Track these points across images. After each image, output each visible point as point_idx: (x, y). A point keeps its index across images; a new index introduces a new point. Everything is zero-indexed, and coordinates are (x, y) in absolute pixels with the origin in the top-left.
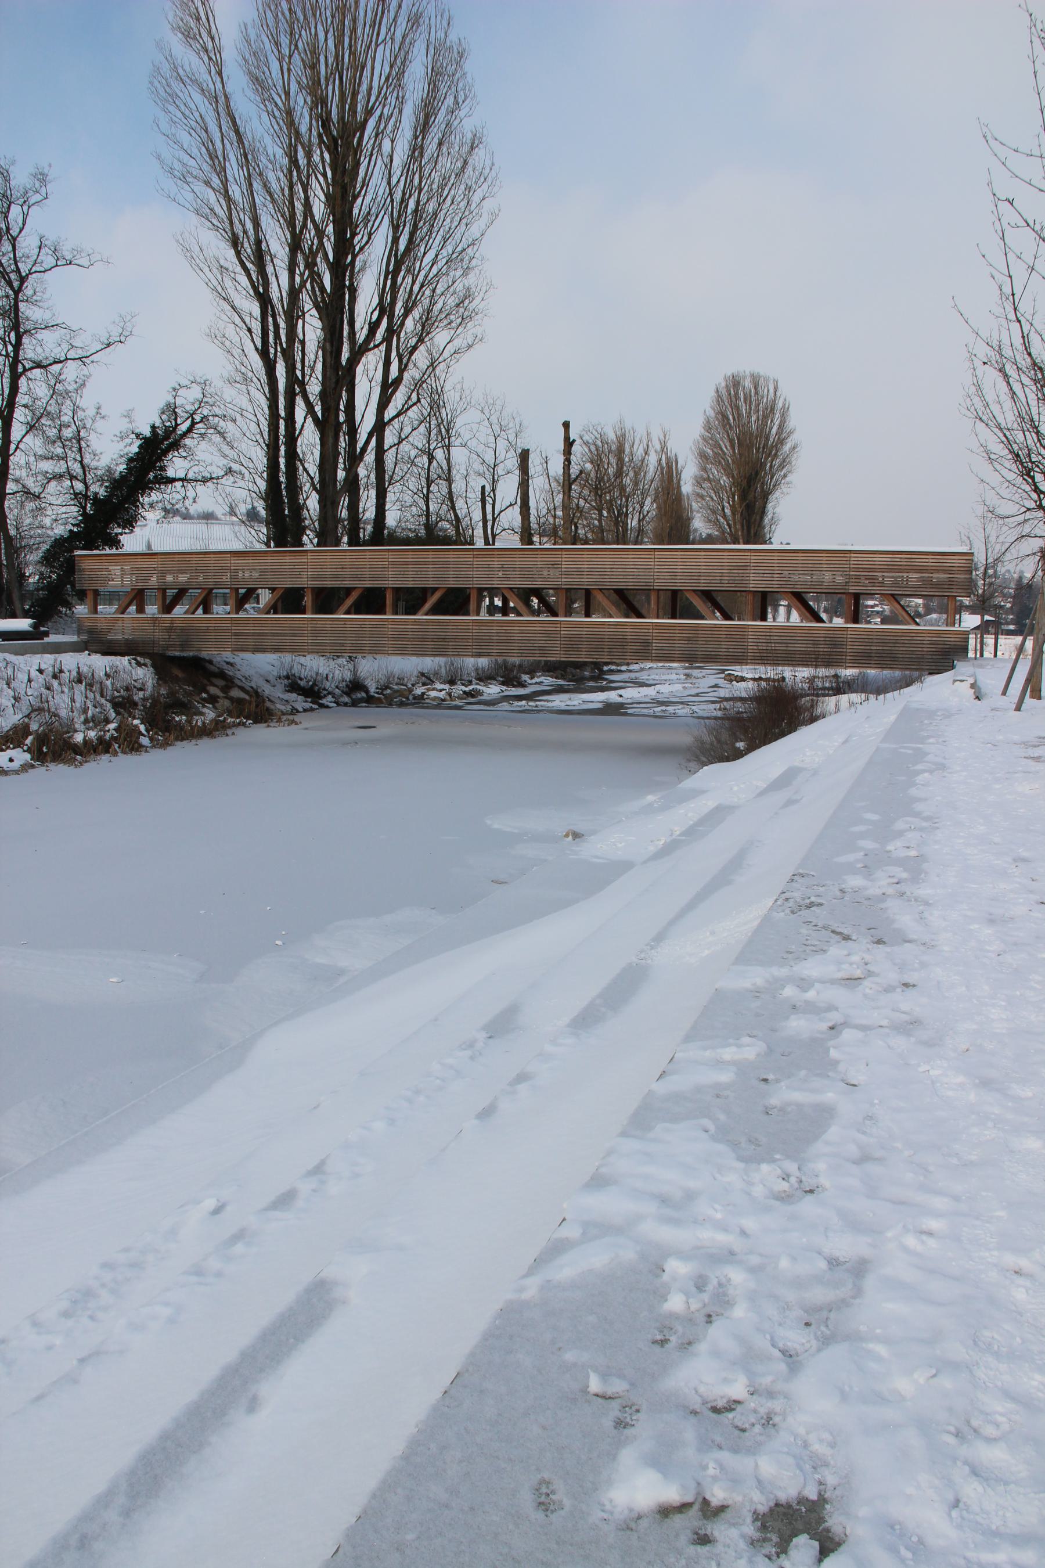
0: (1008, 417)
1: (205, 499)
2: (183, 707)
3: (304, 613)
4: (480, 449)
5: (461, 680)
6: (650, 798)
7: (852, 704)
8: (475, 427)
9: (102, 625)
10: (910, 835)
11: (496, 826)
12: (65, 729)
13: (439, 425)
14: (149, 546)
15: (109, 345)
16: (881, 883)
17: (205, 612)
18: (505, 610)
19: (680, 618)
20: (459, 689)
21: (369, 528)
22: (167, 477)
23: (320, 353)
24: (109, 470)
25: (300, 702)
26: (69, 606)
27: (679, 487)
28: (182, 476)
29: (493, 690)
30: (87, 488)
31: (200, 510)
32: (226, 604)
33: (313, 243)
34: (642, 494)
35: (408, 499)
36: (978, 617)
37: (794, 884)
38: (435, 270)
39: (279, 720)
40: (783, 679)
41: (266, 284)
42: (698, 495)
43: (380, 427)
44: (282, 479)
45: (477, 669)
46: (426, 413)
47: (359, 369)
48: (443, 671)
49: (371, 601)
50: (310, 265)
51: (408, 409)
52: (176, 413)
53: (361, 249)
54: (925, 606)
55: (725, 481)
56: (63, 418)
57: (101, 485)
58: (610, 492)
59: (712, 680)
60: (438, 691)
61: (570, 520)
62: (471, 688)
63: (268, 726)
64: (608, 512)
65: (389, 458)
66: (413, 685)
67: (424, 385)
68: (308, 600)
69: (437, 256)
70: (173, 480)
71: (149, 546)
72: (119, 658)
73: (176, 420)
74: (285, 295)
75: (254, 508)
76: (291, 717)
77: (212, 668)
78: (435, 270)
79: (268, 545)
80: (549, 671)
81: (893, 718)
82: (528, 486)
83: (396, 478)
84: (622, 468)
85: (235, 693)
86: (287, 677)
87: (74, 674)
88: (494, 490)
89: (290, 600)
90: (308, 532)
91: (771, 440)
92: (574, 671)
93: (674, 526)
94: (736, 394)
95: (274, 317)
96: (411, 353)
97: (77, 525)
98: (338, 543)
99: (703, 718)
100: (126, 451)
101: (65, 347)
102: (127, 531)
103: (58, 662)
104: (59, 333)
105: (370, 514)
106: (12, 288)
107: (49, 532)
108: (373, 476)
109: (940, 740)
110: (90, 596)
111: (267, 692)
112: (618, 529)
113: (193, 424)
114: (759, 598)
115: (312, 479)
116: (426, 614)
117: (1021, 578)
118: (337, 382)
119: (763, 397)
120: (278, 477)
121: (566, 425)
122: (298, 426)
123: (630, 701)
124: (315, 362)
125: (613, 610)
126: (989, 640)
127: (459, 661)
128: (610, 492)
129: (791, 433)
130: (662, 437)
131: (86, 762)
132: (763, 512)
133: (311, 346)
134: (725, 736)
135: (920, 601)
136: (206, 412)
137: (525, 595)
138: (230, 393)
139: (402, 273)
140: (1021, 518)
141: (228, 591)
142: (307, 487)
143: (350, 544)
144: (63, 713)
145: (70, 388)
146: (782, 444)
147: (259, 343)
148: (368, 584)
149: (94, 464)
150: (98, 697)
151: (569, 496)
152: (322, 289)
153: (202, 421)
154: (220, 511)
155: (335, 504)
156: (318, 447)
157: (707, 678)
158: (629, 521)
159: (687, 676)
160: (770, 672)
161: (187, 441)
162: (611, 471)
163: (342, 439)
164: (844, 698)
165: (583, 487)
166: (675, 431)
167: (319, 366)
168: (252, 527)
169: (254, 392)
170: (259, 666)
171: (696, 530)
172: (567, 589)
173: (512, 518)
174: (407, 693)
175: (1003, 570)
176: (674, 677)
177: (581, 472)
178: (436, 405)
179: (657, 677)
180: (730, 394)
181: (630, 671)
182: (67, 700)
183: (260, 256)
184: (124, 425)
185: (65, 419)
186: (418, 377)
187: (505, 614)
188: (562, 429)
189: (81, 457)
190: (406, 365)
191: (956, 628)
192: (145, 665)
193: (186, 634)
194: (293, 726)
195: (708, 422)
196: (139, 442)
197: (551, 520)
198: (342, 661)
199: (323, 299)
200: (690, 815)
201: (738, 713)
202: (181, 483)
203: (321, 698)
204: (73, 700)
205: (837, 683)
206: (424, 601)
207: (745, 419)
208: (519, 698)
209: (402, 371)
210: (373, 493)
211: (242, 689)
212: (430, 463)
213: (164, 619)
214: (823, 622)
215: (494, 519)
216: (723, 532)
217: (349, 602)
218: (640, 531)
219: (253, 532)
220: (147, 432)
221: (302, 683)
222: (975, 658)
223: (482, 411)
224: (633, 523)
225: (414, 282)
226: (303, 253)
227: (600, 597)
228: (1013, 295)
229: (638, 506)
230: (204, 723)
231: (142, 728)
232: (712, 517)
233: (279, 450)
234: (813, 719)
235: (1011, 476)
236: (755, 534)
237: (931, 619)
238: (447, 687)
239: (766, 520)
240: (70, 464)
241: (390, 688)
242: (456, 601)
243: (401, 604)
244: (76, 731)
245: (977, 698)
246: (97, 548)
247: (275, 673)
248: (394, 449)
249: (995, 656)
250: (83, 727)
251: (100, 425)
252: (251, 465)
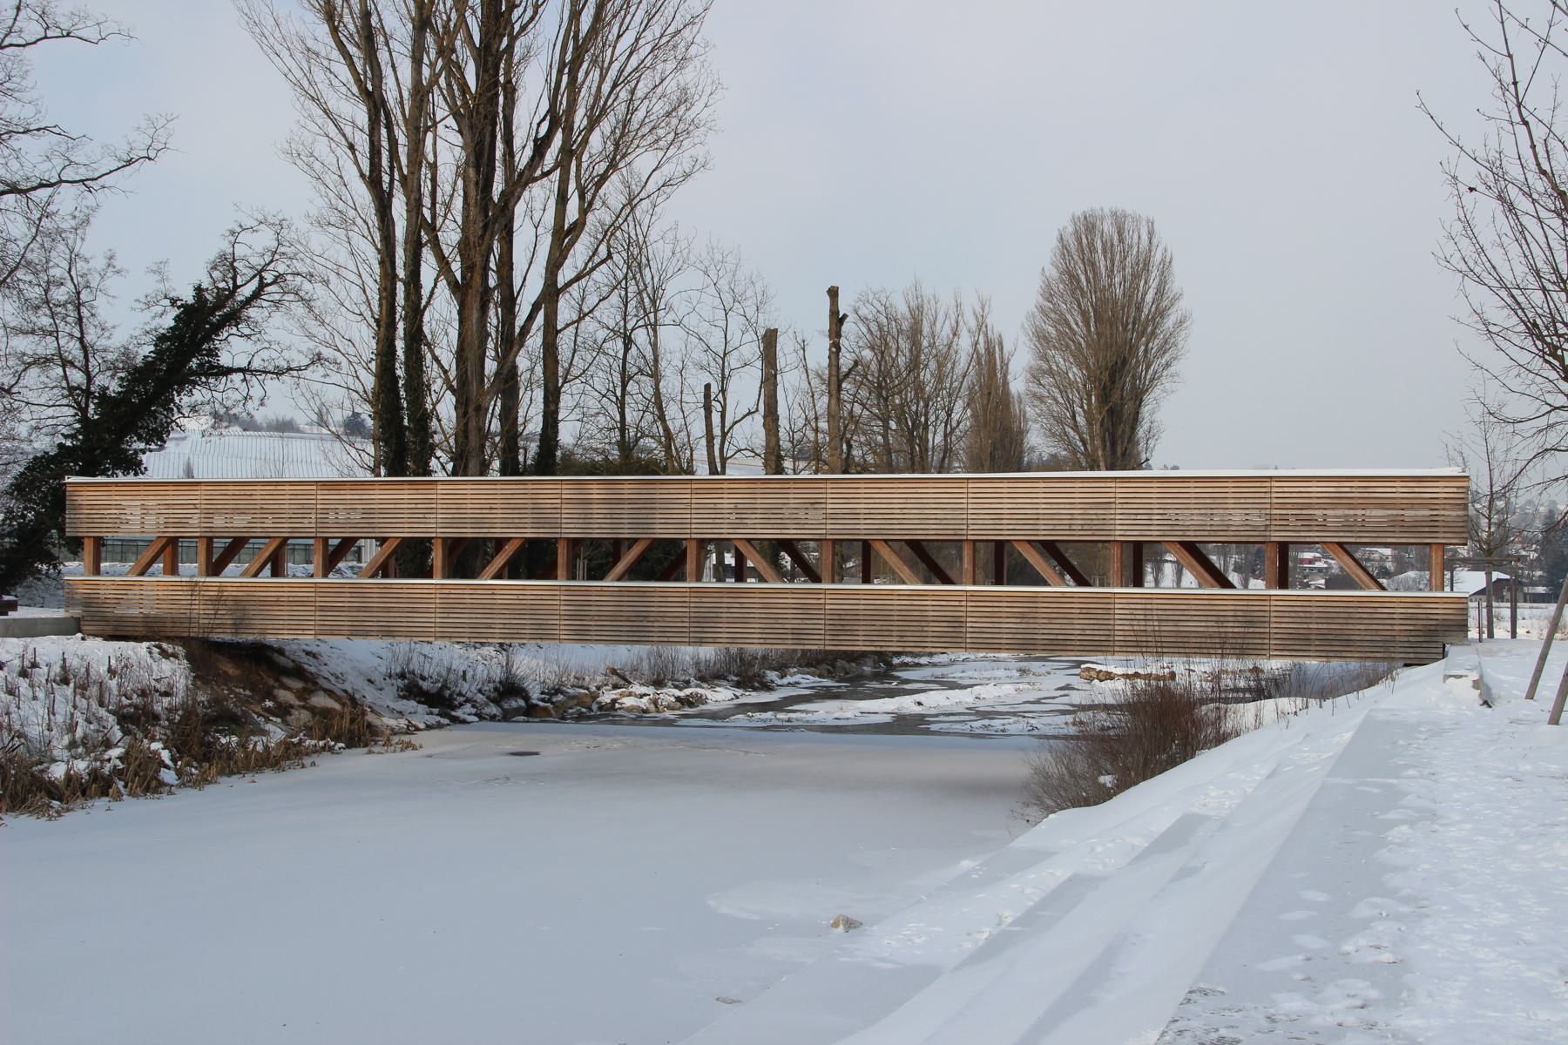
0: (1514, 269)
1: (279, 400)
2: (233, 722)
3: (431, 577)
4: (703, 329)
5: (672, 679)
6: (966, 864)
7: (1281, 715)
8: (695, 295)
9: (103, 593)
10: (1380, 927)
11: (724, 910)
12: (36, 758)
13: (640, 293)
14: (189, 471)
15: (129, 163)
16: (1333, 1008)
17: (275, 574)
18: (740, 573)
19: (1009, 584)
20: (669, 694)
21: (533, 447)
22: (219, 367)
23: (460, 183)
24: (126, 353)
25: (420, 714)
26: (52, 560)
27: (1005, 383)
28: (244, 364)
29: (720, 696)
30: (90, 379)
31: (272, 417)
32: (309, 562)
33: (449, 19)
34: (950, 395)
35: (592, 404)
36: (1482, 575)
37: (1191, 1007)
38: (634, 62)
39: (388, 743)
40: (1173, 675)
41: (378, 77)
42: (1034, 395)
43: (551, 294)
44: (400, 372)
45: (697, 664)
46: (620, 275)
47: (520, 209)
48: (645, 665)
49: (534, 559)
50: (446, 51)
51: (593, 269)
52: (234, 269)
53: (523, 28)
54: (1395, 558)
55: (1075, 373)
56: (52, 272)
57: (113, 377)
58: (900, 393)
59: (1061, 679)
60: (636, 697)
61: (841, 435)
62: (688, 691)
63: (370, 752)
64: (898, 423)
65: (565, 342)
66: (599, 688)
67: (618, 233)
68: (437, 557)
69: (637, 40)
70: (228, 371)
71: (189, 471)
72: (132, 644)
73: (234, 279)
74: (406, 95)
75: (356, 415)
76: (406, 738)
77: (282, 660)
78: (634, 62)
79: (375, 471)
80: (809, 665)
81: (1347, 736)
82: (776, 385)
83: (575, 372)
84: (918, 356)
85: (320, 700)
86: (402, 676)
87: (57, 669)
88: (723, 391)
89: (409, 557)
90: (439, 453)
91: (1146, 311)
92: (847, 665)
93: (1000, 447)
94: (1091, 245)
95: (389, 127)
96: (599, 185)
97: (72, 437)
98: (484, 469)
99: (1048, 737)
100: (154, 324)
101: (59, 162)
102: (153, 446)
103: (30, 651)
104: (47, 140)
105: (535, 425)
107: (24, 446)
108: (539, 370)
109: (1426, 772)
110: (89, 546)
111: (369, 699)
112: (913, 448)
113: (262, 285)
114: (1130, 551)
115: (445, 372)
116: (619, 579)
117: (1551, 513)
118: (485, 228)
119: (1131, 247)
120: (393, 369)
121: (833, 293)
122: (425, 292)
123: (933, 712)
124: (452, 196)
125: (905, 571)
126: (1503, 610)
127: (668, 651)
128: (900, 393)
129: (1175, 299)
130: (978, 309)
131: (68, 810)
132: (1135, 419)
133: (446, 173)
134: (1081, 766)
135: (1387, 552)
136: (281, 268)
137: (774, 548)
138: (319, 241)
139: (585, 65)
140: (1543, 422)
141: (311, 541)
142: (437, 385)
143: (503, 472)
144: (34, 731)
145: (64, 226)
146: (1162, 317)
148: (530, 533)
149: (101, 343)
150: (95, 705)
151: (839, 399)
152: (464, 87)
154: (301, 420)
155: (481, 410)
156: (456, 324)
157: (1050, 679)
158: (930, 436)
159: (1023, 671)
160: (1153, 666)
161: (252, 312)
162: (901, 361)
163: (492, 312)
164: (1269, 705)
165: (859, 385)
166: (998, 298)
167: (458, 203)
168: (352, 445)
169: (357, 239)
170: (357, 658)
171: (1032, 449)
172: (834, 541)
173: (751, 432)
174: (588, 700)
175: (1521, 501)
176: (1001, 673)
177: (856, 363)
178: (636, 265)
179: (976, 675)
180: (1080, 243)
181: (934, 665)
182: (43, 711)
183: (369, 36)
184: (151, 285)
185: (57, 272)
186: (608, 221)
187: (740, 579)
188: (827, 299)
189: (82, 332)
190: (591, 204)
191: (1447, 593)
192: (175, 656)
193: (240, 607)
194: (410, 753)
195: (1049, 286)
196: (176, 312)
197: (811, 436)
198: (489, 651)
199: (465, 103)
200: (1028, 891)
201: (1103, 729)
202: (241, 376)
203: (454, 708)
204: (52, 712)
205: (1258, 680)
206: (617, 559)
207: (1105, 281)
208: (764, 707)
209: (584, 211)
210: (539, 394)
211: (330, 693)
212: (627, 350)
213: (206, 585)
214: (1232, 586)
215: (724, 435)
216: (1074, 452)
217: (499, 561)
218: (947, 450)
219: (353, 452)
220: (188, 297)
221: (425, 685)
222: (1480, 640)
223: (706, 273)
224: (936, 438)
225: (602, 79)
226: (436, 33)
227: (885, 553)
228: (1515, 83)
229: (943, 414)
230: (266, 747)
231: (165, 755)
232: (1057, 429)
233: (395, 329)
234: (1221, 739)
235: (1524, 358)
236: (1124, 454)
237: (1406, 579)
238: (650, 690)
239: (1141, 433)
240: (62, 342)
241: (562, 693)
242: (665, 560)
243: (581, 565)
244: (54, 761)
245: (1486, 703)
246: (103, 473)
247: (383, 670)
248: (572, 329)
249: (1514, 635)
250: (66, 754)
251: (112, 283)
252: (352, 351)
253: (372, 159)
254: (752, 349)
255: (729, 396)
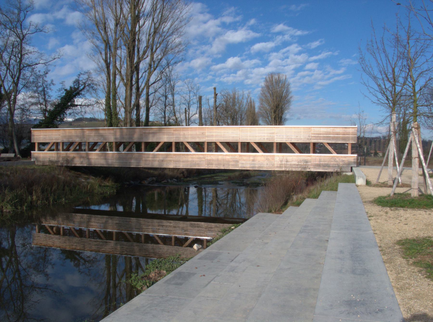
4: (184, 95)
73: (79, 85)
106: (19, 38)
136: (90, 83)
147: (104, 57)
149: (49, 100)
153: (88, 86)
162: (231, 104)
184: (60, 86)
220: (68, 88)
251: (52, 87)
253: (105, 55)
254: (195, 99)
255: (190, 110)
